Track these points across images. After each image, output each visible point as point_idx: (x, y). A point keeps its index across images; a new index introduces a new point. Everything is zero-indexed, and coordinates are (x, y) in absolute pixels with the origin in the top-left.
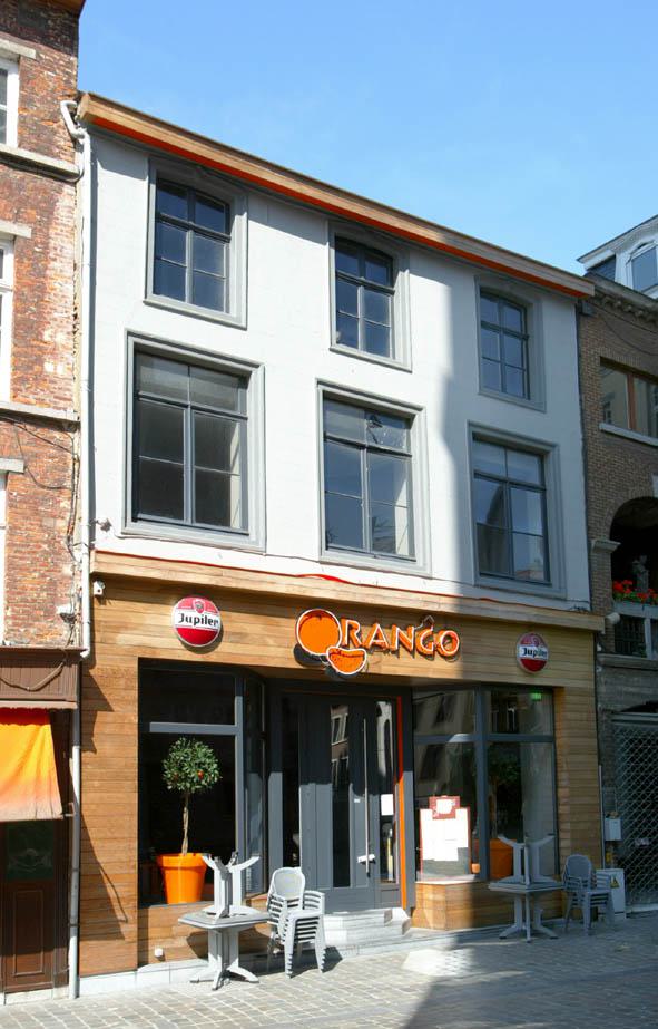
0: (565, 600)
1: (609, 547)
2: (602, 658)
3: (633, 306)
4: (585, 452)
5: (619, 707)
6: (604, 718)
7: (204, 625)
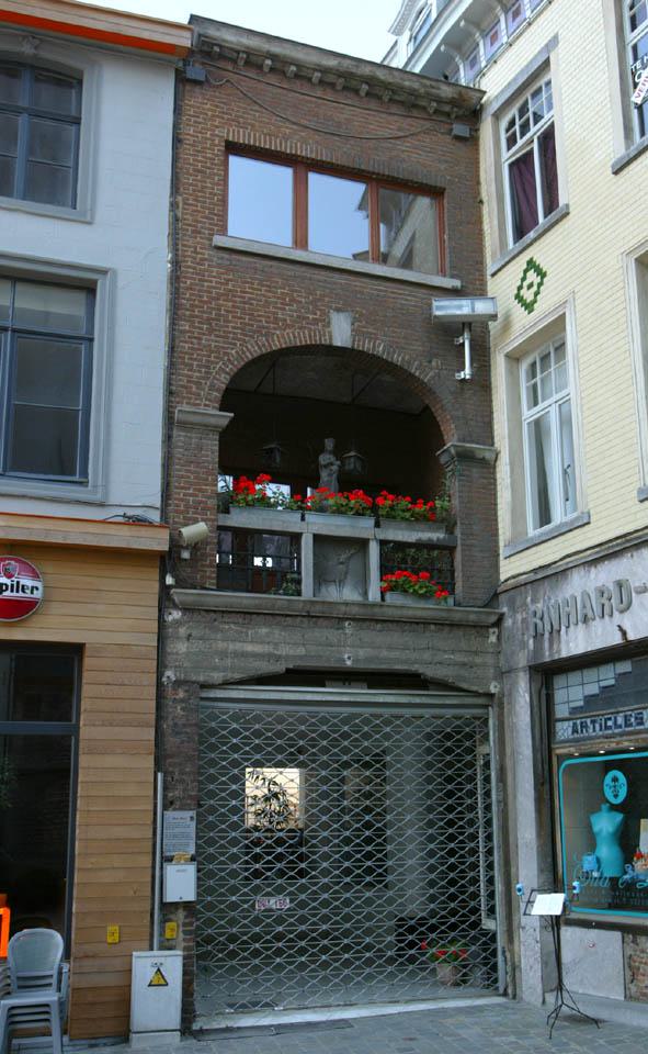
0: (102, 505)
1: (213, 421)
2: (178, 595)
3: (320, 71)
4: (175, 278)
5: (217, 677)
6: (181, 694)
7: (15, 594)
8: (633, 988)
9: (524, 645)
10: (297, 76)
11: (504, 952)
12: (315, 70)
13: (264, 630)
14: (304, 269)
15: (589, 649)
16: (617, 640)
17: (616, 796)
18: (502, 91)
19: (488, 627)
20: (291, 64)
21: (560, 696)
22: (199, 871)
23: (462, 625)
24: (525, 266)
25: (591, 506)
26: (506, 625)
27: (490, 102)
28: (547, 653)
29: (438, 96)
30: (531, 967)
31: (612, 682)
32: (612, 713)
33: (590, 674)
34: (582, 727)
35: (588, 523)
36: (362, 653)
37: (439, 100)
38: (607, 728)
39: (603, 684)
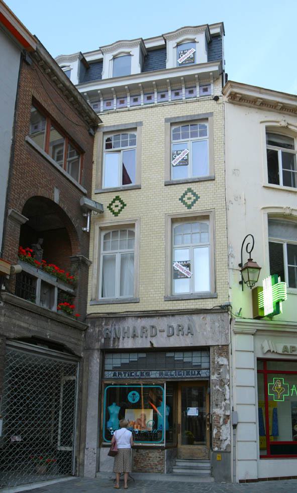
5: (12, 335)
8: (135, 468)
9: (99, 340)
10: (54, 81)
11: (76, 459)
12: (61, 83)
13: (27, 318)
14: (49, 165)
15: (134, 347)
16: (149, 346)
17: (134, 400)
18: (110, 126)
19: (83, 330)
20: (61, 83)
21: (108, 361)
22: (3, 423)
23: (63, 323)
24: (115, 198)
25: (140, 296)
26: (89, 331)
27: (103, 127)
28: (112, 345)
29: (90, 115)
30: (90, 464)
31: (136, 360)
32: (135, 371)
33: (127, 356)
34: (119, 374)
35: (139, 302)
36: (52, 334)
37: (90, 117)
38: (131, 376)
39: (131, 360)
